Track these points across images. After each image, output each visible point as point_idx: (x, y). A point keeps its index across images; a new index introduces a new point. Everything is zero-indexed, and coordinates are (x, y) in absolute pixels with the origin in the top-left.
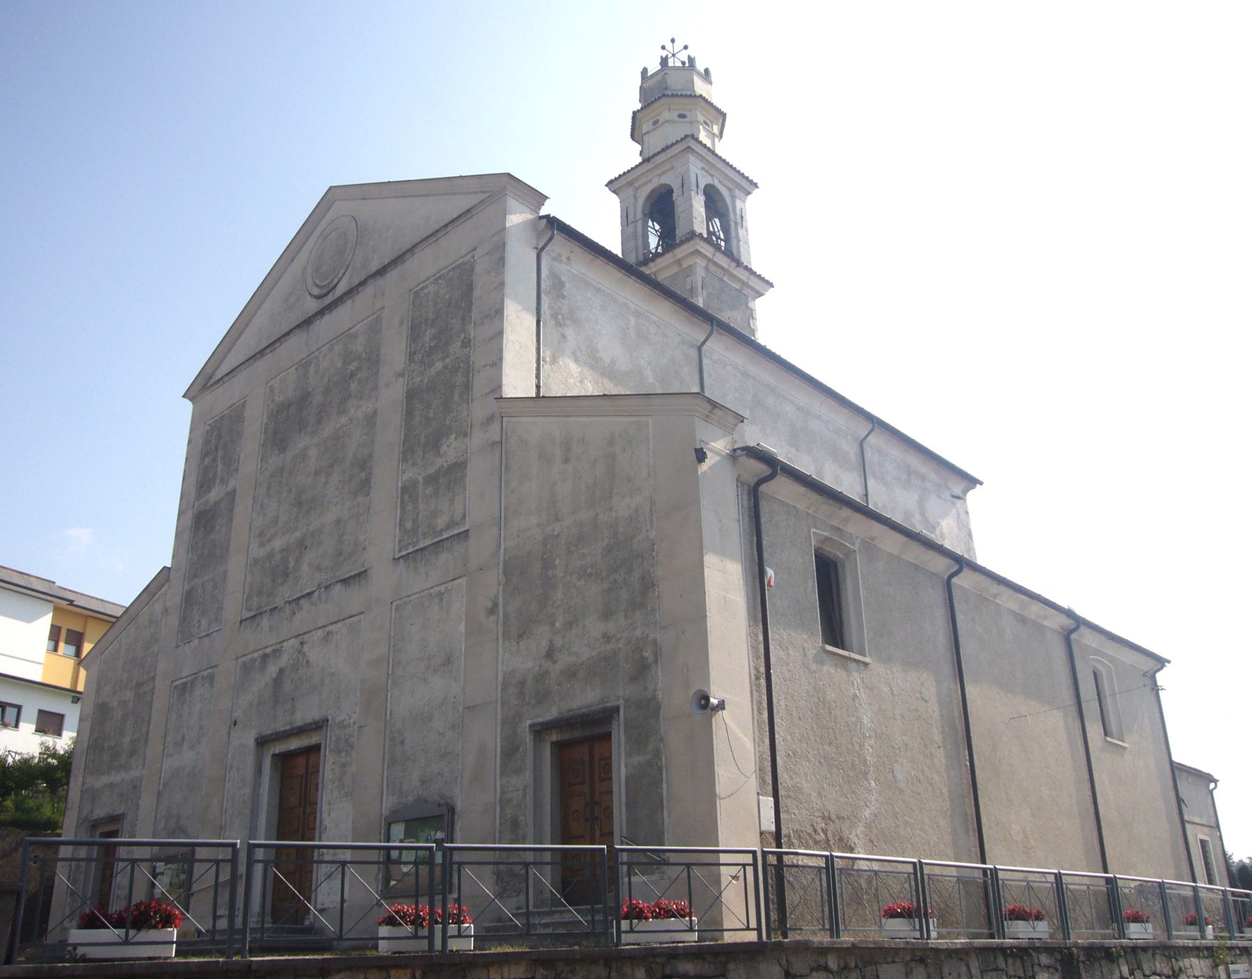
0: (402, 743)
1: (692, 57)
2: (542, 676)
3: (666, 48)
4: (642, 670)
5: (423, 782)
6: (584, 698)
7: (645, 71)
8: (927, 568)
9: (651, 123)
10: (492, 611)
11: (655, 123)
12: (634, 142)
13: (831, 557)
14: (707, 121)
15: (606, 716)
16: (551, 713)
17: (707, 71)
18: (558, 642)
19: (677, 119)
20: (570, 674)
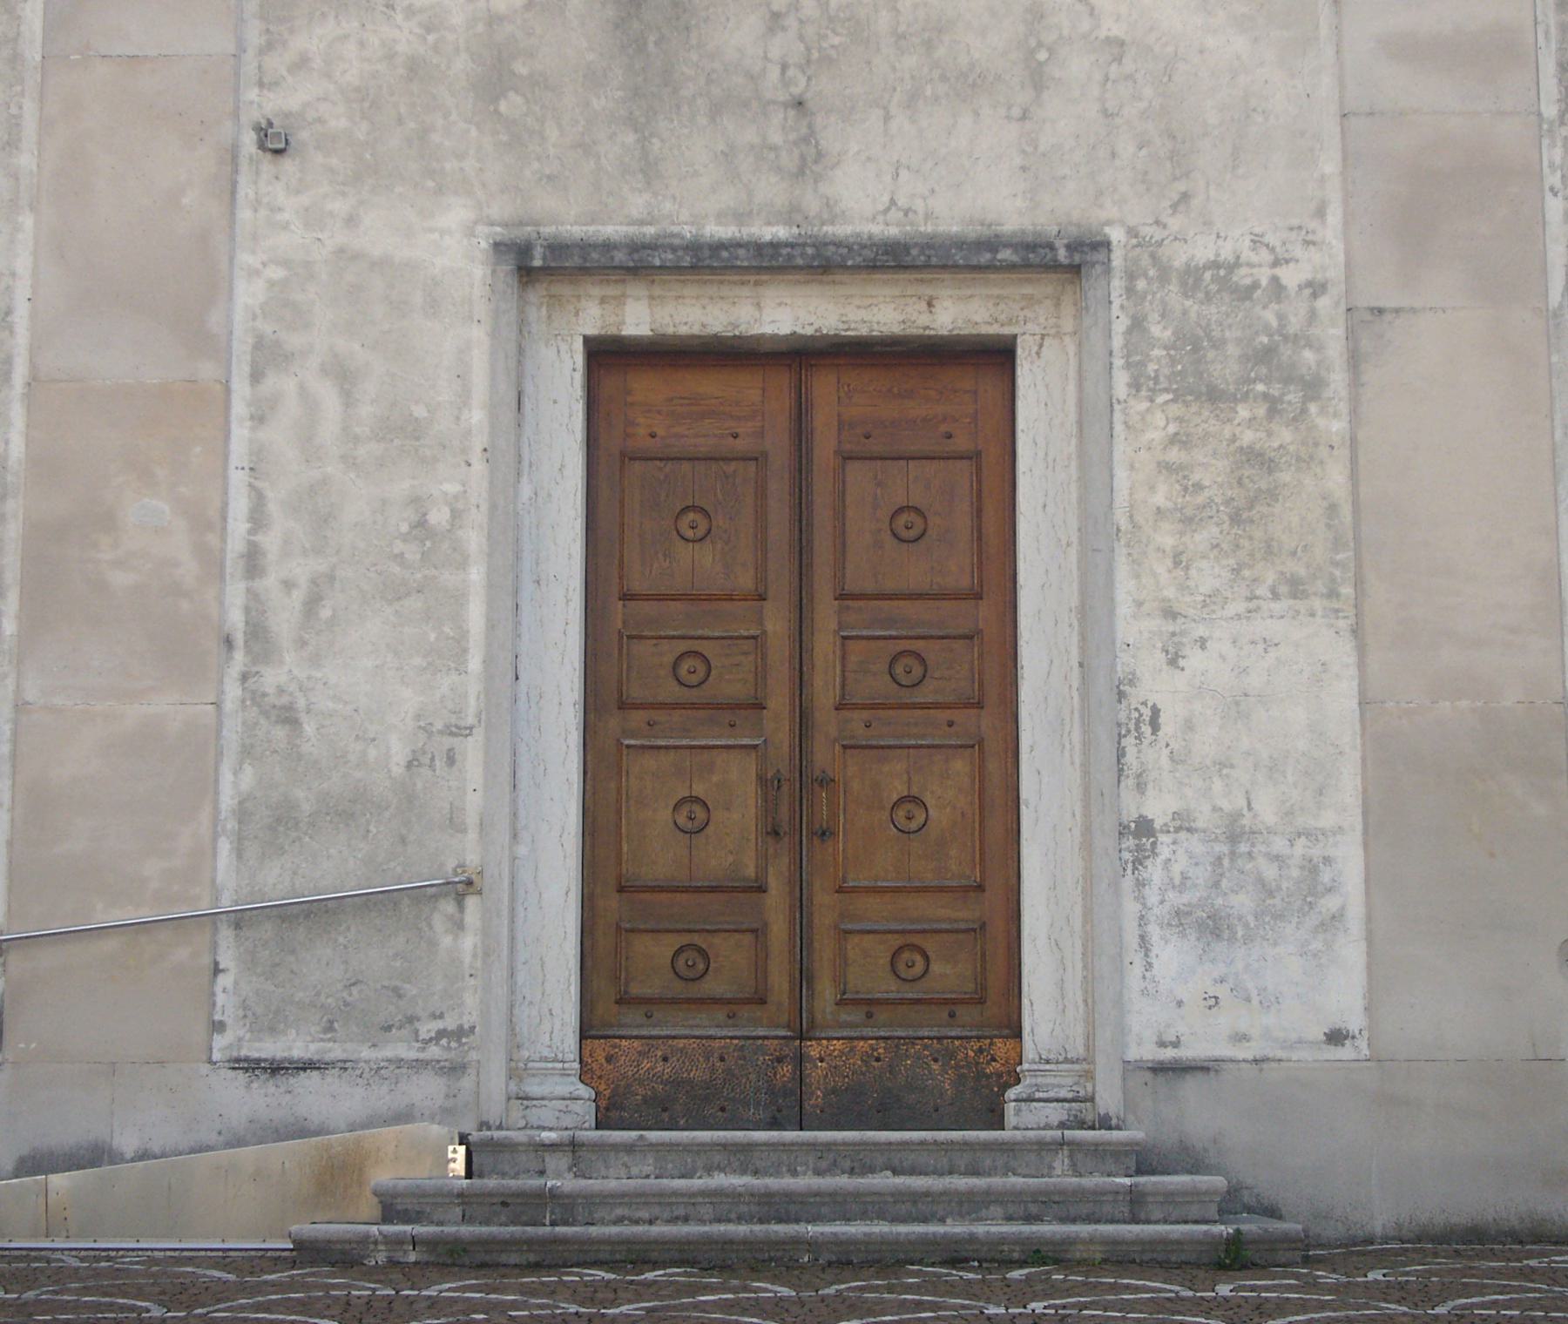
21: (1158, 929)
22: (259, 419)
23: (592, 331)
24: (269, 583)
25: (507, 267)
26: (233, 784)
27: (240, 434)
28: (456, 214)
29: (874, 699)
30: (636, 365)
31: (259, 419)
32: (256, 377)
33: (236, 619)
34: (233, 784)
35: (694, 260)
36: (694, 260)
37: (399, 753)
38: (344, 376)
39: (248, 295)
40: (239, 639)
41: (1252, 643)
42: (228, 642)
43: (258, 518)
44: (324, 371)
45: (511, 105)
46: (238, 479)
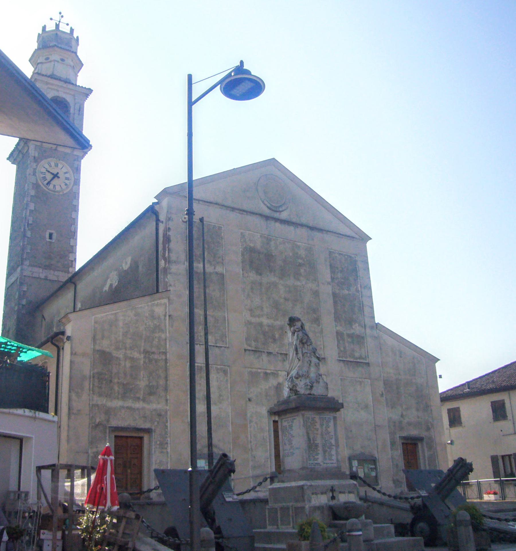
0: (351, 431)
1: (73, 28)
2: (400, 422)
3: (66, 25)
4: (428, 429)
5: (362, 447)
6: (414, 432)
7: (44, 28)
8: (391, 463)
9: (45, 58)
10: (382, 395)
11: (47, 59)
12: (30, 63)
13: (143, 468)
14: (75, 66)
15: (421, 439)
16: (405, 434)
17: (78, 37)
18: (404, 413)
19: (60, 61)
20: (409, 424)
21: (311, 461)
22: (250, 428)
23: (274, 419)
24: (252, 444)
25: (269, 414)
26: (251, 463)
27: (249, 429)
28: (264, 408)
29: (187, 236)
30: (319, 395)
31: (250, 428)
32: (250, 423)
33: (250, 447)
34: (251, 463)
35: (297, 259)
36: (297, 259)
37: (263, 460)
38: (256, 423)
39: (249, 415)
40: (250, 449)
41: (63, 277)
42: (249, 450)
43: (251, 438)
44: (449, 411)
45: (268, 398)
46: (249, 433)
